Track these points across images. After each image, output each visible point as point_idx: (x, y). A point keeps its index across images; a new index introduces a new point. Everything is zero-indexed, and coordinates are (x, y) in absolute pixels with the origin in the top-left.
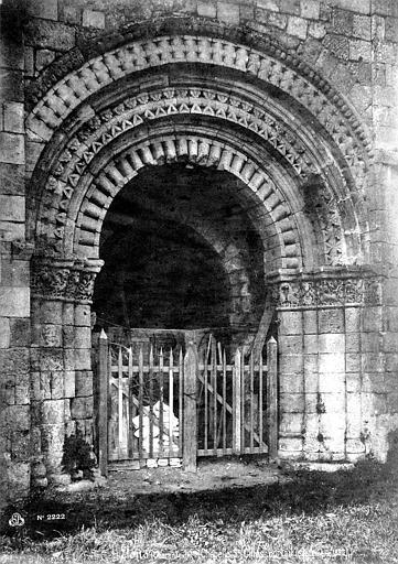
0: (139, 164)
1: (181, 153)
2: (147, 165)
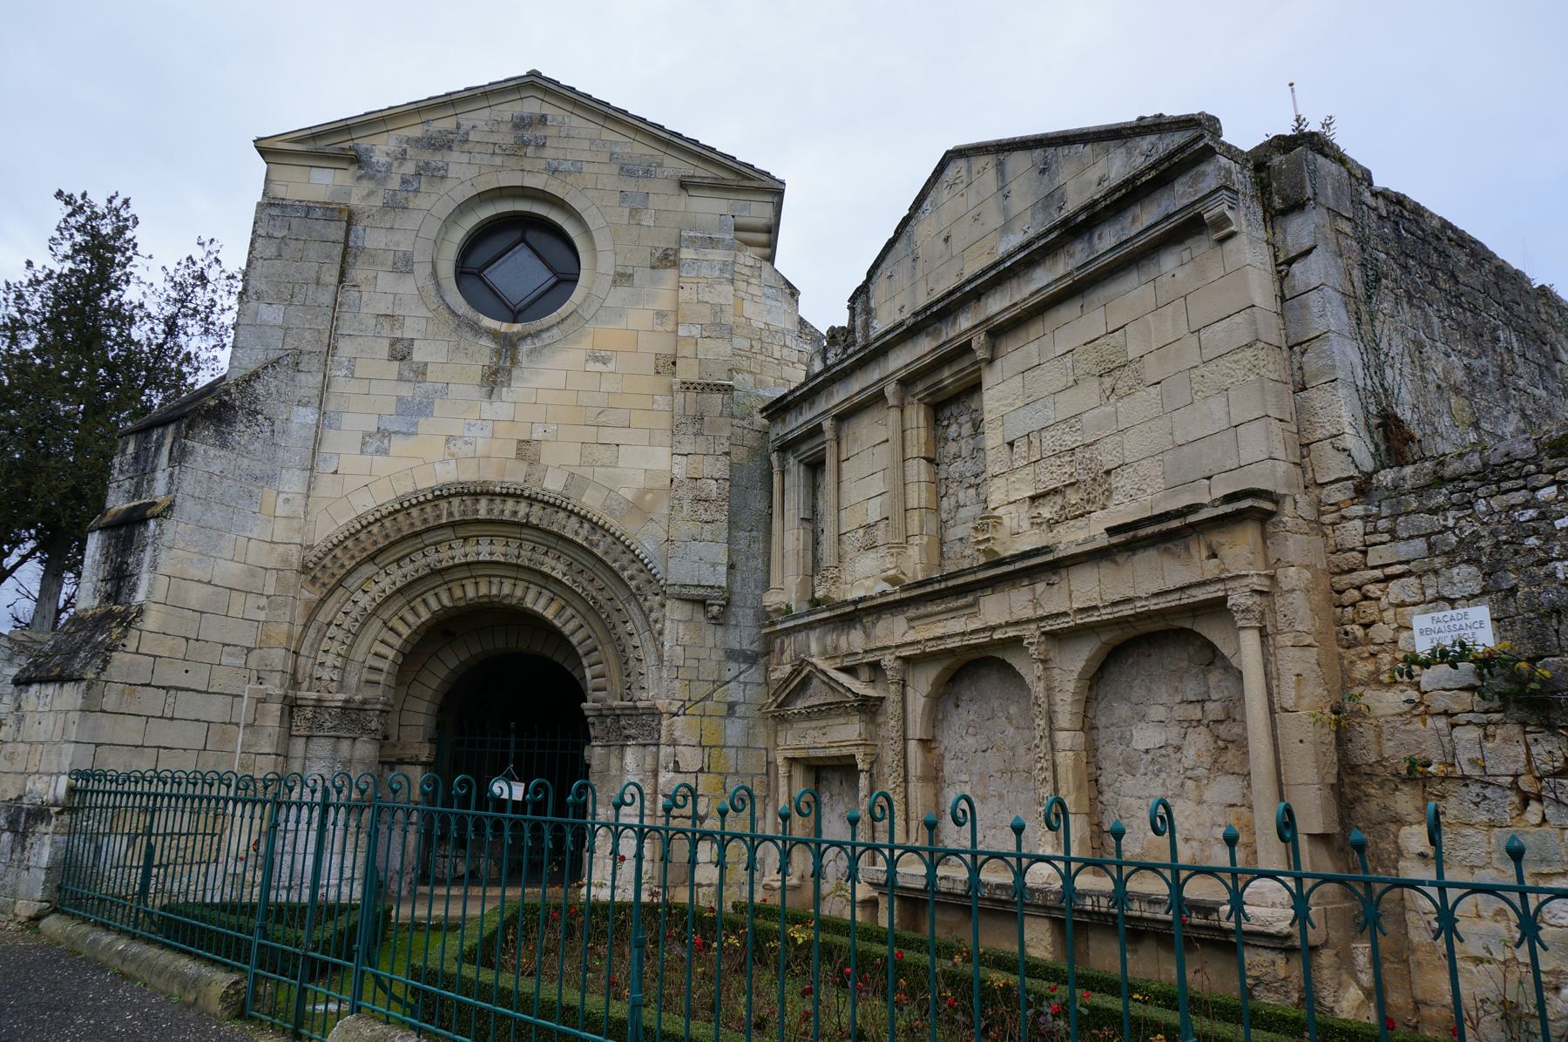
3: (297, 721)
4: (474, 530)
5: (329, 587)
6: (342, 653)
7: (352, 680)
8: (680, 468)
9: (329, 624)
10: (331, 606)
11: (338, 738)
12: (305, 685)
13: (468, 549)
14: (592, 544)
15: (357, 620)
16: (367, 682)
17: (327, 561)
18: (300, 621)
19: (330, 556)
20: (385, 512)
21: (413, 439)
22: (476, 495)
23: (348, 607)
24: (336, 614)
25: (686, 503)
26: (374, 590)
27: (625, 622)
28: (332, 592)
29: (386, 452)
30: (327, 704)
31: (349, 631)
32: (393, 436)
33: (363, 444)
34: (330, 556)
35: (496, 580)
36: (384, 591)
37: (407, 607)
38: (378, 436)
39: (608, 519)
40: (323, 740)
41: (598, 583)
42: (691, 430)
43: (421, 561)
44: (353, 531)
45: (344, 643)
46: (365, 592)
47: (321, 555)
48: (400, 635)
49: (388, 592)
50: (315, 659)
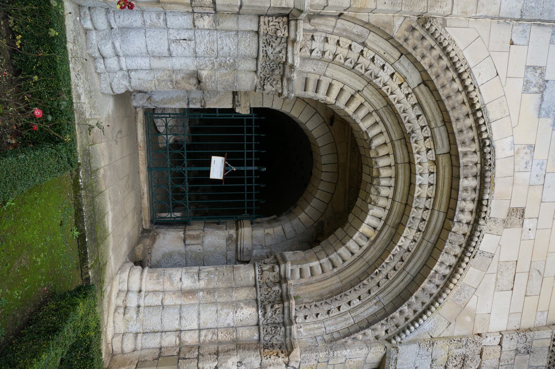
0: (372, 133)
1: (381, 171)
2: (371, 140)
3: (274, 21)
4: (445, 173)
5: (405, 45)
6: (337, 59)
7: (309, 67)
8: (491, 341)
9: (364, 44)
10: (383, 46)
11: (257, 59)
12: (308, 26)
13: (426, 165)
14: (432, 277)
15: (366, 70)
16: (307, 79)
17: (429, 41)
18: (373, 19)
19: (433, 44)
20: (473, 95)
21: (535, 114)
22: (482, 176)
23: (379, 61)
24: (373, 50)
25: (463, 350)
26: (393, 85)
27: (359, 298)
28: (398, 46)
29: (526, 90)
30: (290, 48)
31: (357, 64)
32: (539, 95)
33: (534, 68)
34: (433, 44)
35: (392, 182)
36: (392, 93)
37: (371, 109)
38: (541, 81)
39: (454, 292)
40: (255, 46)
41: (393, 274)
42: (520, 346)
43: (417, 125)
44: (458, 65)
45: (346, 59)
46: (392, 76)
47: (437, 35)
48: (347, 104)
49: (391, 97)
50: (332, 34)
